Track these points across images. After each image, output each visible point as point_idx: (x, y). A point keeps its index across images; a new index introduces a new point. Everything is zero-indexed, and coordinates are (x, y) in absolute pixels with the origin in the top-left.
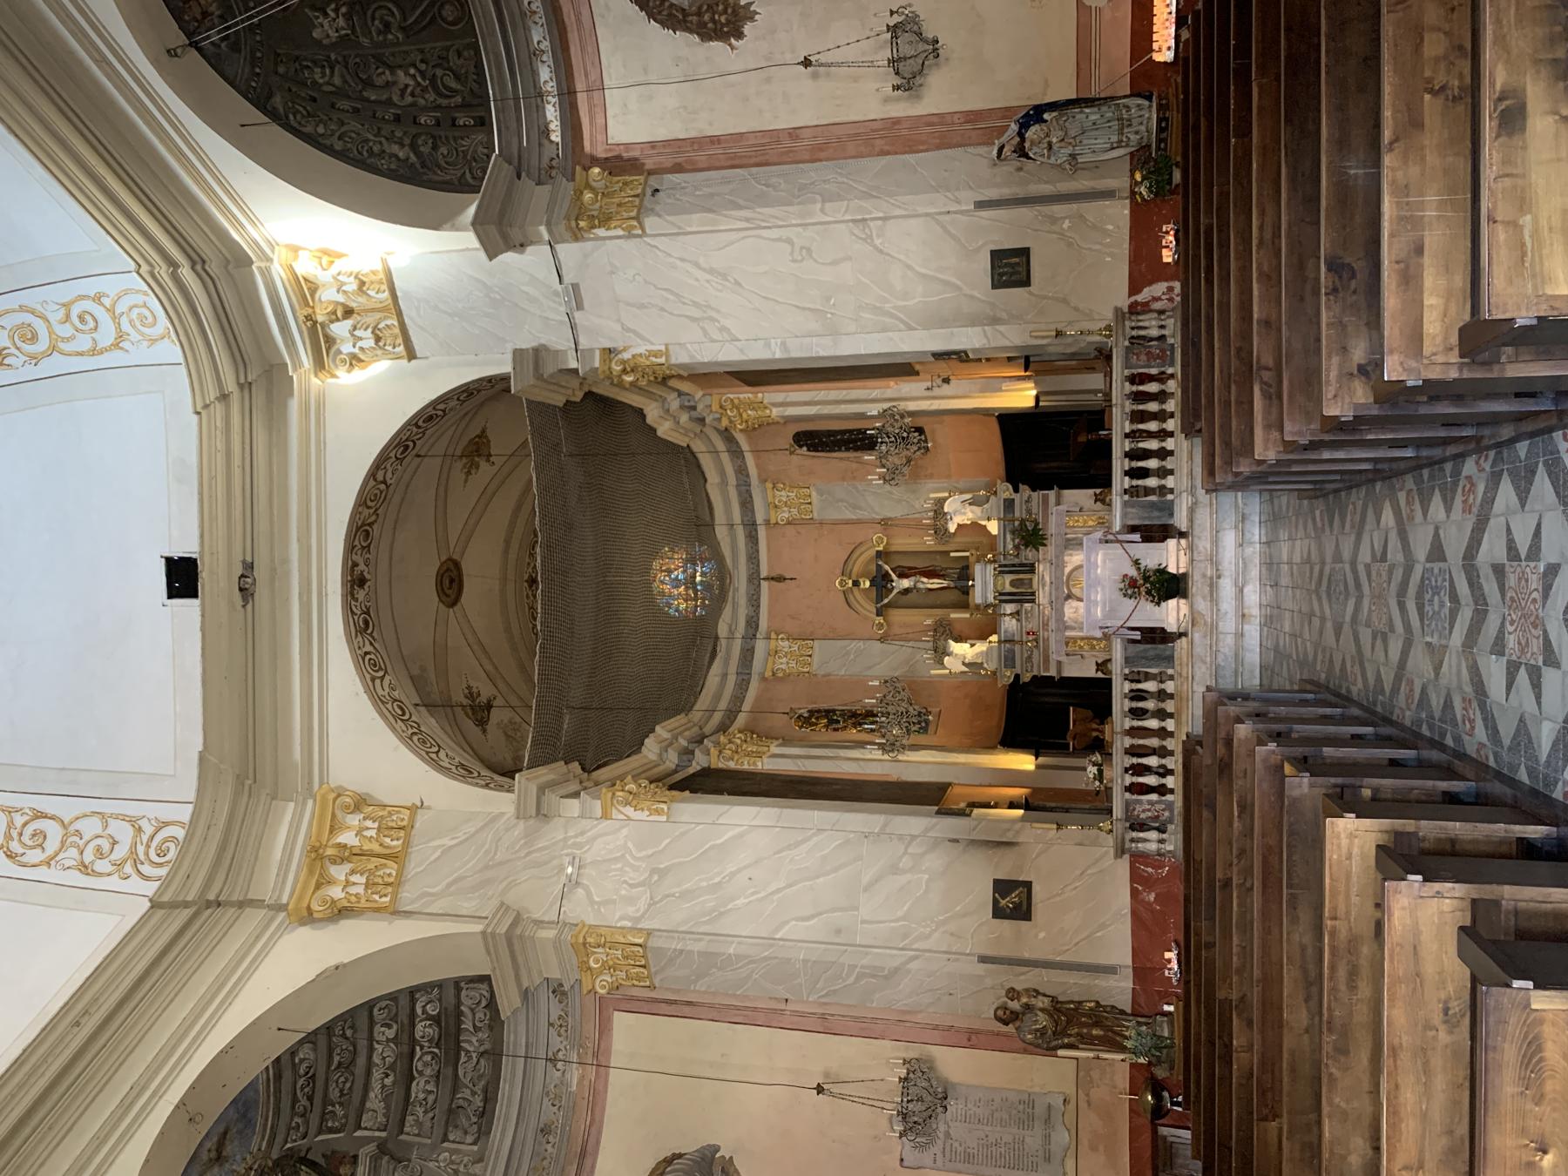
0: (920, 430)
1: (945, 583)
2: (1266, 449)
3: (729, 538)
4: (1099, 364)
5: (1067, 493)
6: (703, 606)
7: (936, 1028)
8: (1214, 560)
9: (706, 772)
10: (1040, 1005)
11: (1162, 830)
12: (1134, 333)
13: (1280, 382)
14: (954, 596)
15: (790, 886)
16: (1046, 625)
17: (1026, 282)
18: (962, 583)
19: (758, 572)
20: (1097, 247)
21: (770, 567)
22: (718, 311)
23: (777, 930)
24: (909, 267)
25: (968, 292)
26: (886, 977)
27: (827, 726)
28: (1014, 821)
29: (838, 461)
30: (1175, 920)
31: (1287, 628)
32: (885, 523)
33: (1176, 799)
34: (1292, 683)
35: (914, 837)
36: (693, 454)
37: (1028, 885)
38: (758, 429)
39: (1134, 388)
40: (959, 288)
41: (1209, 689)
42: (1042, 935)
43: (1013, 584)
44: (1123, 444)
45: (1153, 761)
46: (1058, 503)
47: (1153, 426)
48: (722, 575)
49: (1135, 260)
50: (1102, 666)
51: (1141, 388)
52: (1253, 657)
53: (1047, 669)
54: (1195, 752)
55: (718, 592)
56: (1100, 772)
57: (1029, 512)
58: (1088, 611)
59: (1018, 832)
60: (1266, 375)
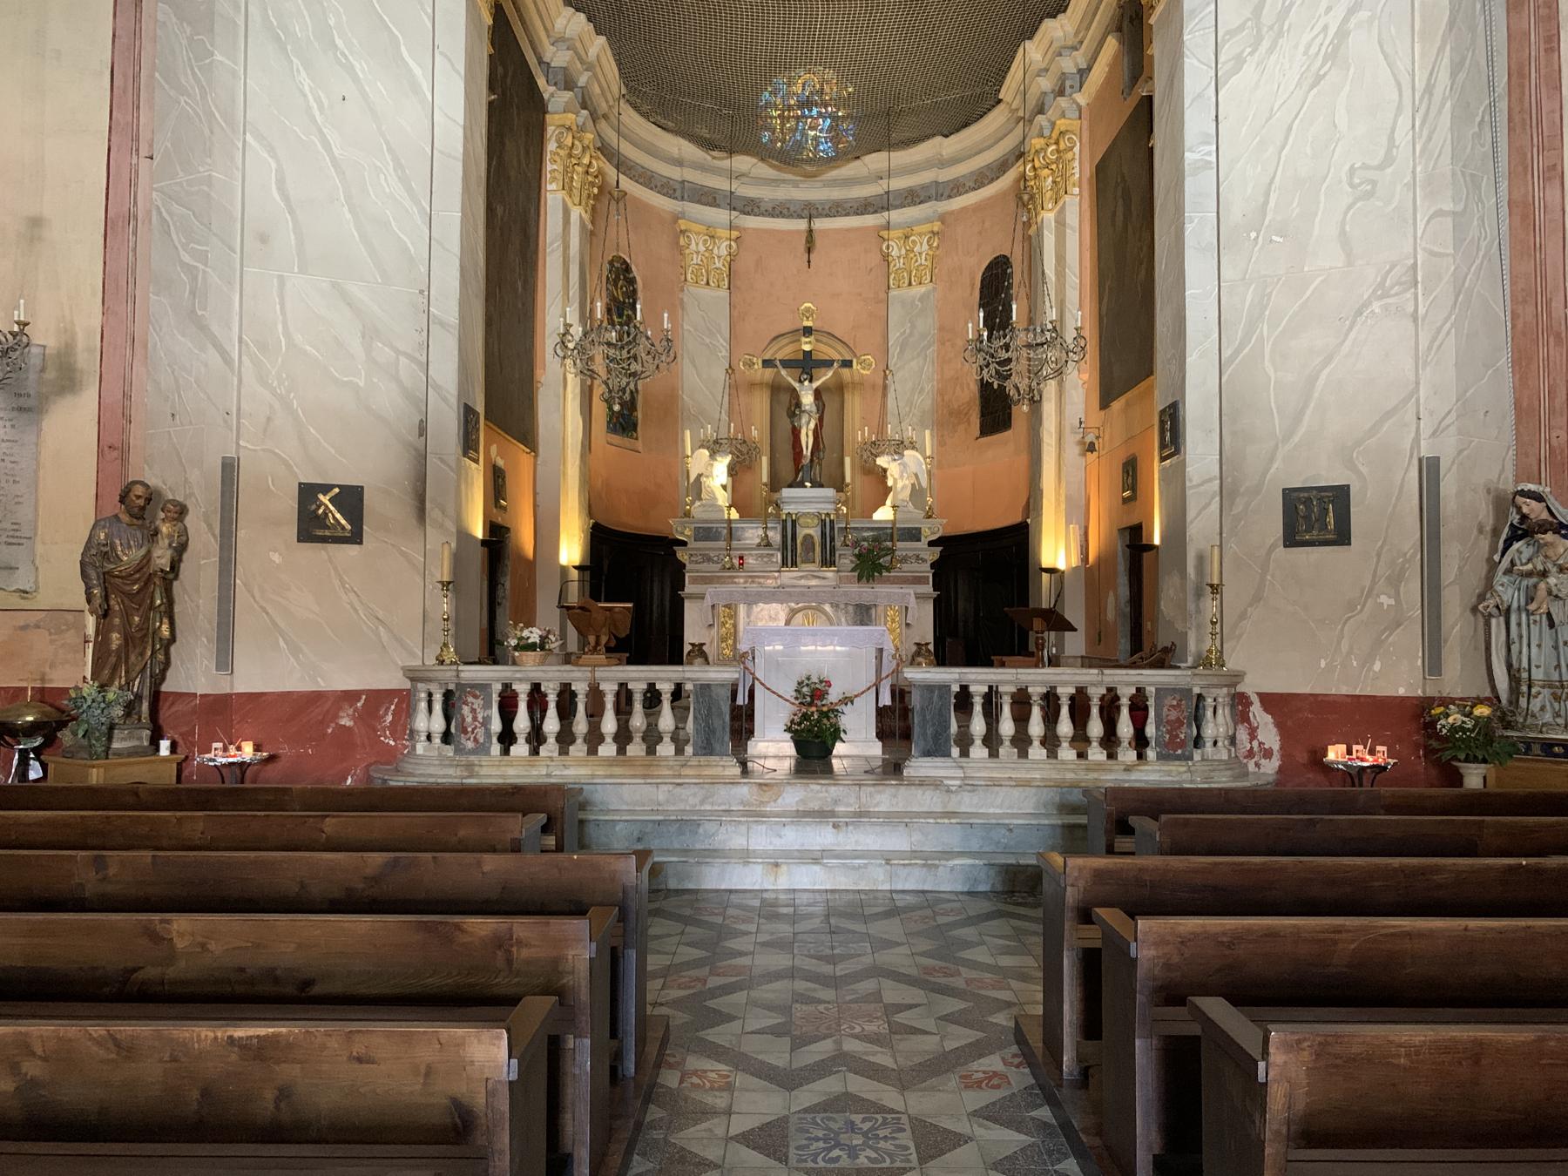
1: (807, 452)
5: (929, 608)
7: (127, 396)
9: (537, 106)
10: (157, 553)
11: (447, 737)
12: (1209, 701)
15: (335, 162)
19: (820, 216)
20: (1345, 646)
21: (825, 232)
24: (1328, 360)
26: (193, 311)
37: (356, 538)
38: (1024, 199)
39: (1125, 701)
42: (276, 558)
43: (808, 537)
44: (1128, 684)
50: (699, 651)
53: (694, 581)
55: (789, 158)
56: (532, 647)
57: (904, 560)
58: (775, 633)
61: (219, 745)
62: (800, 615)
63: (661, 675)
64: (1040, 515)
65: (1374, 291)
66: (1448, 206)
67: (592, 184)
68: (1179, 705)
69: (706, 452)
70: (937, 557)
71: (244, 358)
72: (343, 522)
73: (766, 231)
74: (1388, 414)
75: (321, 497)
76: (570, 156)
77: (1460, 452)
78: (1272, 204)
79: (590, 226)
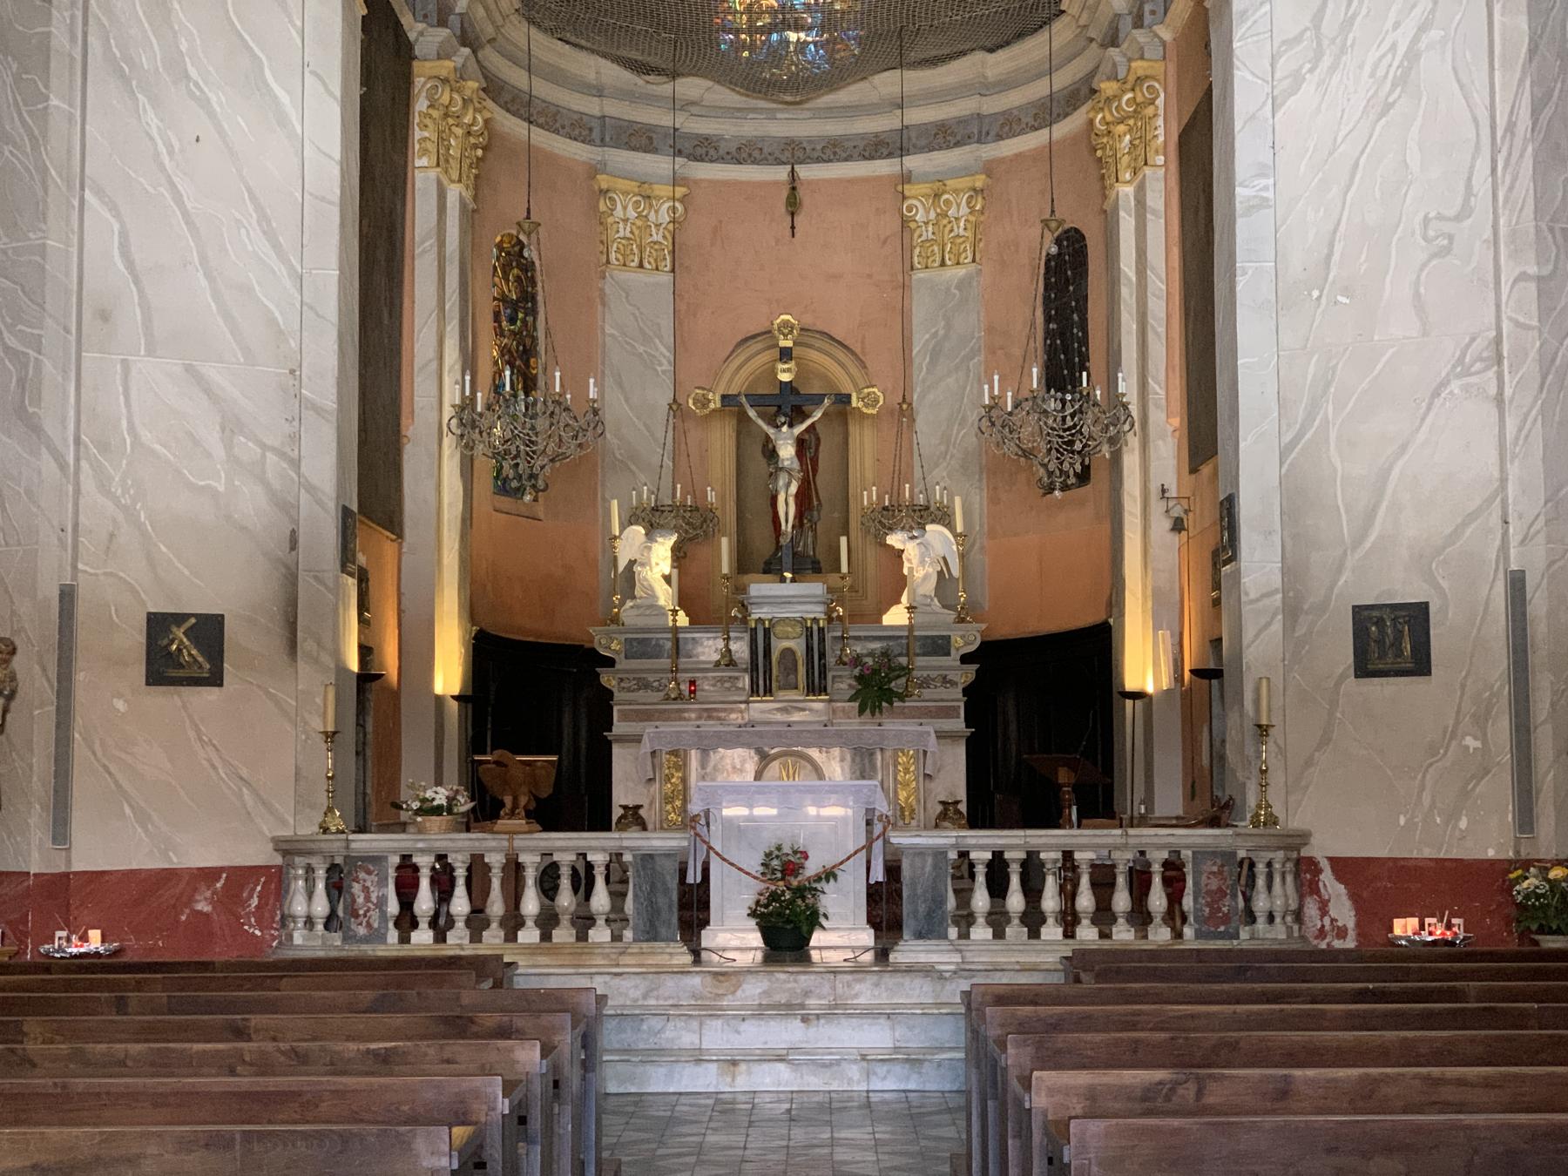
0: (1084, 477)
1: (787, 527)
2: (1050, 1091)
3: (881, 97)
4: (1203, 806)
5: (960, 752)
6: (738, 46)
8: (836, 1011)
9: (403, 52)
11: (331, 921)
12: (1261, 868)
13: (1175, 1113)
14: (762, 544)
15: (186, 214)
16: (709, 714)
17: (1364, 669)
18: (787, 560)
20: (1426, 799)
21: (815, 184)
22: (1333, 68)
23: (99, 192)
24: (1403, 448)
25: (1349, 563)
26: (22, 407)
27: (503, 299)
28: (337, 655)
29: (1025, 314)
30: (160, 948)
31: (712, 1138)
32: (903, 412)
33: (391, 945)
34: (612, 1148)
35: (296, 464)
36: (1047, 22)
37: (216, 679)
39: (1156, 868)
40: (1358, 542)
41: (601, 999)
42: (120, 705)
43: (788, 653)
44: (1049, 848)
45: (460, 904)
46: (940, 735)
47: (1085, 901)
48: (798, 86)
49: (1401, 869)
51: (1157, 881)
52: (658, 1081)
53: (625, 717)
54: (481, 977)
55: (770, 79)
56: (437, 811)
57: (925, 683)
59: (316, 661)
60: (1188, 1092)
61: (64, 934)
62: (776, 764)
63: (594, 843)
64: (1122, 615)
65: (1454, 367)
66: (1533, 270)
67: (475, 147)
68: (1220, 872)
69: (640, 530)
70: (971, 677)
71: (84, 464)
72: (200, 659)
73: (726, 183)
74: (1471, 517)
75: (174, 629)
76: (446, 115)
77: (1553, 562)
78: (1336, 257)
79: (472, 206)
